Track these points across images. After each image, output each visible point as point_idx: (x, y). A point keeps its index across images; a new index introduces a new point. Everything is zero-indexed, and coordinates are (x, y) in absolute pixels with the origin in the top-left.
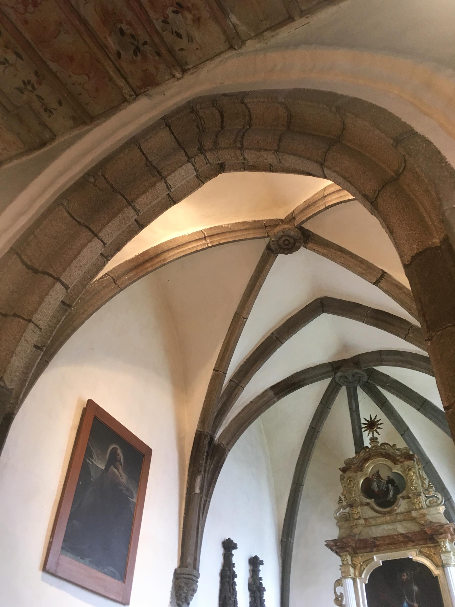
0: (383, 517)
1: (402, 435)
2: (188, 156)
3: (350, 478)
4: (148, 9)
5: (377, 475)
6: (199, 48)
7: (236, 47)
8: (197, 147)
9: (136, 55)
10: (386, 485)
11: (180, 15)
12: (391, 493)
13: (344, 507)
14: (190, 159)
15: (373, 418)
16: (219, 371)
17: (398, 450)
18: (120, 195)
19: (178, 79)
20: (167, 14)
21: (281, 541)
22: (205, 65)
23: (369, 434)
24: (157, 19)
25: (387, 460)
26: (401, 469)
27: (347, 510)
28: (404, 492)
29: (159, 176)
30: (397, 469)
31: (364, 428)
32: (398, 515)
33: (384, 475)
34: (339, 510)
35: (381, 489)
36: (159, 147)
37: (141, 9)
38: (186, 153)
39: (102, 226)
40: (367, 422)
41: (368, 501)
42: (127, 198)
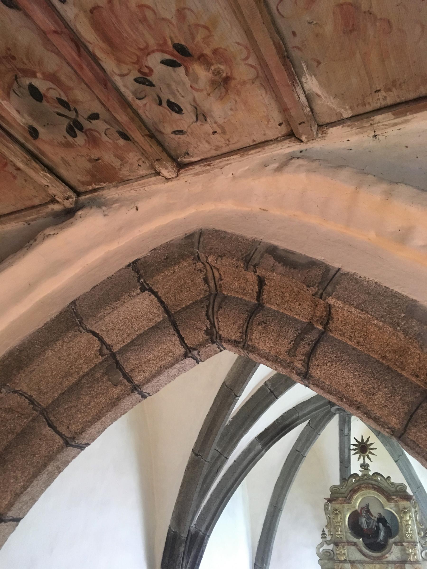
0: (372, 563)
1: (396, 461)
2: (186, 344)
3: (336, 510)
4: (98, 53)
5: (367, 509)
6: (219, 131)
7: (303, 138)
8: (205, 328)
9: (74, 136)
10: (377, 524)
11: (181, 70)
12: (382, 534)
13: (328, 542)
14: (190, 351)
15: (365, 440)
16: (200, 455)
17: (392, 484)
18: (47, 427)
19: (167, 179)
20: (147, 67)
21: (255, 564)
22: (229, 162)
23: (359, 459)
24: (122, 76)
25: (379, 494)
26: (394, 508)
27: (331, 547)
28: (397, 537)
29: (127, 383)
30: (390, 507)
31: (353, 449)
32: (390, 565)
33: (375, 511)
34: (321, 545)
35: (370, 526)
36: (127, 318)
37: (80, 55)
38: (182, 339)
39: (12, 495)
40: (357, 443)
41: (356, 540)
42: (63, 433)
